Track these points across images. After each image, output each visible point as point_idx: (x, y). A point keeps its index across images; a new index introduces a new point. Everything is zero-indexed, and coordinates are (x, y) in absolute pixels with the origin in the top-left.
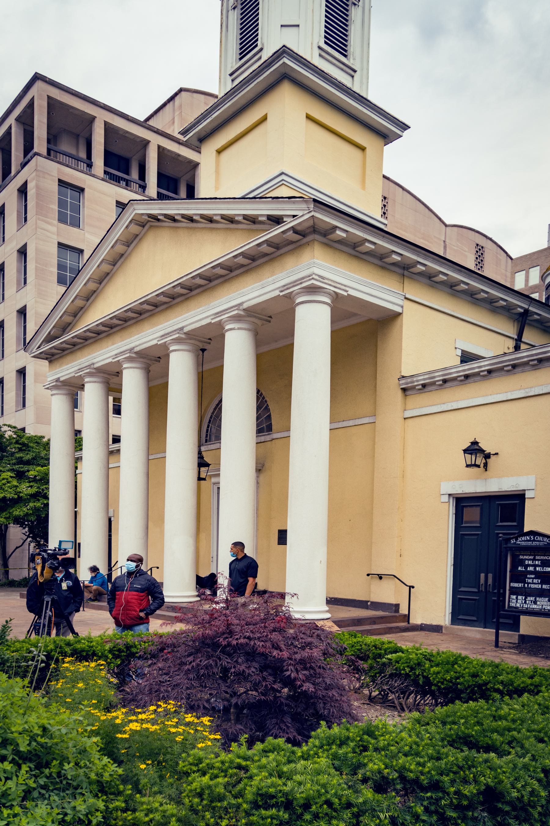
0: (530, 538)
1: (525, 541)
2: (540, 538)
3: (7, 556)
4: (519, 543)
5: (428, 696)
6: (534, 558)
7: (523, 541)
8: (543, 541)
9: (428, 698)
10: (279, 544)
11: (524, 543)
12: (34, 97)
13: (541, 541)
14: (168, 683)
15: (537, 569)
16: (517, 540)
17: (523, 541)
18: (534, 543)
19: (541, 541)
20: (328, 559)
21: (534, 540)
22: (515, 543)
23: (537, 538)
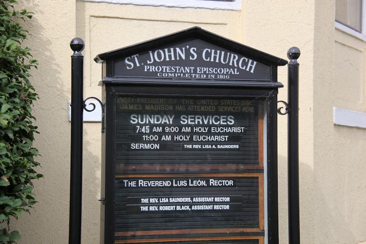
0: (188, 54)
1: (170, 63)
2: (217, 55)
3: (84, 100)
4: (153, 69)
5: (145, 209)
6: (160, 137)
7: (164, 63)
8: (227, 66)
9: (149, 204)
13: (220, 65)
15: (167, 201)
17: (164, 63)
19: (220, 65)
20: (315, 93)
21: (200, 62)
22: (138, 71)
23: (208, 55)
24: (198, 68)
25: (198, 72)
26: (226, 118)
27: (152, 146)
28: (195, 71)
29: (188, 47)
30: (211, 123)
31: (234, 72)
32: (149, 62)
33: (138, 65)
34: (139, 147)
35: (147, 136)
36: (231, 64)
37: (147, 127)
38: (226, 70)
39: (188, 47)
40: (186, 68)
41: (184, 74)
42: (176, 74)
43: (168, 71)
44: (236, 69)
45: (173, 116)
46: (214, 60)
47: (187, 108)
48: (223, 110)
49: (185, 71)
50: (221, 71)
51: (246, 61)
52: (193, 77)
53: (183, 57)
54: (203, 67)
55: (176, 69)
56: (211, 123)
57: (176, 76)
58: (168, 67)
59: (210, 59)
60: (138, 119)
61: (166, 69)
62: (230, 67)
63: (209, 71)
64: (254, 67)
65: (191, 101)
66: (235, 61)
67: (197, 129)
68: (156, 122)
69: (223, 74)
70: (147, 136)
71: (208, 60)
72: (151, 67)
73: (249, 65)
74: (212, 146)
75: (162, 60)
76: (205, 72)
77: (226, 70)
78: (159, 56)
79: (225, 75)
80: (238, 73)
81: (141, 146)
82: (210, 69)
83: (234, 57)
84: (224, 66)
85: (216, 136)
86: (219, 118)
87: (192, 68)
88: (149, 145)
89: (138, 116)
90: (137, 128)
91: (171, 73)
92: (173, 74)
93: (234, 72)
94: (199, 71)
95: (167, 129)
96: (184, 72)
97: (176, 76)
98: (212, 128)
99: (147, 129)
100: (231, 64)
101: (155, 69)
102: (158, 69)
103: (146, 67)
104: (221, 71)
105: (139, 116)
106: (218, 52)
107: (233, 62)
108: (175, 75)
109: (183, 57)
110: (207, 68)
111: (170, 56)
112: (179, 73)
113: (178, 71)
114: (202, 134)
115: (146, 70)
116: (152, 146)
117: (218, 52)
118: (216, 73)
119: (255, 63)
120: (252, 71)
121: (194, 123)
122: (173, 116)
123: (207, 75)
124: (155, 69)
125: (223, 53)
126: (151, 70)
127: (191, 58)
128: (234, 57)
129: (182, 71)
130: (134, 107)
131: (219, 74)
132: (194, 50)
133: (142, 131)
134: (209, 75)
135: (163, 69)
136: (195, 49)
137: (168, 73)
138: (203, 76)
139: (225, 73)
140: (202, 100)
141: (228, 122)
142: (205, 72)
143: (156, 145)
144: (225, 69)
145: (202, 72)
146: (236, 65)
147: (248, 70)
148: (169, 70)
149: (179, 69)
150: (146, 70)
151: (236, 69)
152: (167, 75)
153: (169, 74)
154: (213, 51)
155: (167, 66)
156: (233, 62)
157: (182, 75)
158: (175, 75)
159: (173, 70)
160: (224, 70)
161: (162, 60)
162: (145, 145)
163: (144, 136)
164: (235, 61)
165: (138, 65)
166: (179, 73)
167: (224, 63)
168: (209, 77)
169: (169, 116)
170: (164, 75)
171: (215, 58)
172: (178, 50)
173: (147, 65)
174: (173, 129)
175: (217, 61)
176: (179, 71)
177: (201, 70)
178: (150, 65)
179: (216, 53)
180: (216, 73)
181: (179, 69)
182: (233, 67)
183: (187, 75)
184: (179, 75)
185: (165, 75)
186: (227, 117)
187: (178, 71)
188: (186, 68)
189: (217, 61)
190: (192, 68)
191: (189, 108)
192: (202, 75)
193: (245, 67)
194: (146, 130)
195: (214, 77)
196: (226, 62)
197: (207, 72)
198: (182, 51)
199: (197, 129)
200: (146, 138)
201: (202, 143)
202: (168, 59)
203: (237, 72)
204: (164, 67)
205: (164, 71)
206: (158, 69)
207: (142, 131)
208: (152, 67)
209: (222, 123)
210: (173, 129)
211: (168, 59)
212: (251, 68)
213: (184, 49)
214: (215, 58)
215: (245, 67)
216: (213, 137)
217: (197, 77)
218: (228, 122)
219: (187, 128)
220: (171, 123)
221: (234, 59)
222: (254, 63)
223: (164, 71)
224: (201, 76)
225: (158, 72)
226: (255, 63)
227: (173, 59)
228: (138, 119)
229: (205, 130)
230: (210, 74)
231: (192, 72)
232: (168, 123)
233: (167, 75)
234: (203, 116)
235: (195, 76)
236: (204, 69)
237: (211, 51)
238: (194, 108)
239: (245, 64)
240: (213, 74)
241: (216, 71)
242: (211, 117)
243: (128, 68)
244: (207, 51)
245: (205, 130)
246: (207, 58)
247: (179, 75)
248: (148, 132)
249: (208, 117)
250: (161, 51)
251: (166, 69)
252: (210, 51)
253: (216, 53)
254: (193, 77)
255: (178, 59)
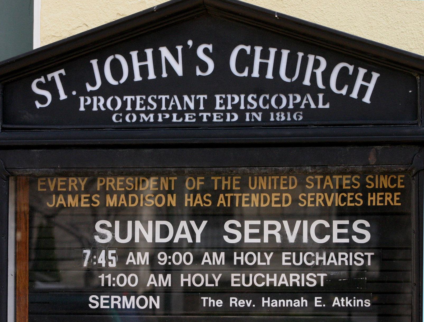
0: (191, 60)
1: (145, 88)
2: (270, 62)
4: (99, 104)
7: (131, 87)
8: (297, 88)
10: (338, 225)
11: (139, 109)
12: (292, 235)
14: (385, 8)
16: (77, 79)
17: (131, 87)
18: (227, 107)
19: (277, 86)
21: (223, 81)
23: (245, 61)
24: (218, 97)
25: (218, 108)
26: (350, 227)
27: (142, 302)
28: (210, 105)
29: (190, 43)
30: (305, 240)
31: (316, 103)
32: (89, 88)
33: (63, 96)
34: (109, 304)
35: (109, 276)
36: (307, 82)
37: (110, 252)
38: (295, 98)
39: (190, 43)
40: (186, 98)
41: (181, 114)
42: (160, 115)
43: (138, 108)
44: (321, 96)
45: (204, 223)
46: (260, 72)
47: (215, 199)
48: (314, 202)
49: (182, 106)
50: (279, 102)
51: (351, 73)
52: (205, 120)
53: (179, 69)
54: (293, 93)
55: (159, 102)
56: (305, 240)
57: (160, 120)
58: (138, 98)
59: (251, 71)
60: (112, 230)
61: (134, 103)
62: (303, 91)
63: (246, 102)
64: (371, 86)
65: (235, 182)
66: (319, 73)
67: (244, 259)
68: (159, 240)
69: (286, 110)
70: (109, 276)
71: (245, 74)
72: (95, 99)
73: (359, 82)
74: (311, 301)
75: (123, 81)
76: (236, 108)
77: (295, 98)
78: (116, 70)
79: (292, 111)
80: (327, 106)
81: (113, 302)
82: (250, 99)
83: (317, 64)
84: (288, 89)
85: (291, 275)
86: (327, 225)
87: (201, 97)
88: (133, 298)
89: (113, 224)
90: (86, 254)
91: (147, 113)
92: (151, 116)
93: (316, 103)
94: (221, 105)
95: (162, 256)
96: (179, 108)
97: (160, 120)
98: (284, 254)
99: (110, 257)
100: (307, 82)
101: (105, 105)
102: (114, 103)
103: (82, 99)
104: (279, 102)
105: (117, 223)
106: (273, 51)
107: (314, 75)
108: (156, 118)
109: (179, 69)
110: (243, 96)
111: (144, 70)
112: (167, 111)
113: (164, 108)
114: (255, 268)
115: (82, 109)
116: (142, 302)
117: (273, 51)
118: (267, 107)
119: (375, 76)
120: (367, 99)
121: (258, 241)
122: (204, 223)
123: (242, 114)
124: (105, 105)
125: (285, 53)
126: (95, 109)
127: (199, 73)
128: (317, 64)
129: (175, 106)
130: (80, 200)
131: (275, 111)
132: (206, 51)
133: (99, 262)
134: (248, 114)
135: (124, 104)
136: (210, 47)
137: (138, 113)
138: (232, 117)
139: (291, 106)
140: (382, 178)
141: (355, 238)
142: (236, 108)
143: (151, 298)
144: (291, 96)
145: (229, 107)
146: (320, 84)
147: (354, 95)
148: (141, 106)
149: (168, 102)
150: (82, 109)
151: (321, 96)
152: (135, 119)
153: (143, 115)
154: (258, 49)
155: (135, 95)
156: (314, 75)
157: (175, 115)
158: (156, 118)
159: (152, 106)
160: (98, 107)
161: (123, 81)
162: (125, 298)
163: (102, 276)
164: (319, 73)
165: (63, 96)
166: (167, 111)
167: (288, 80)
168: (248, 119)
169: (193, 223)
170: (127, 119)
171: (263, 67)
172: (165, 52)
173: (84, 96)
174: (177, 257)
175: (269, 76)
176: (167, 106)
177: (226, 101)
178: (92, 94)
179: (265, 55)
180: (267, 107)
181: (168, 102)
182: (313, 90)
183: (187, 115)
184: (167, 116)
185: (131, 118)
186: (351, 223)
187: (164, 108)
188: (186, 98)
189: (269, 76)
190: (202, 97)
191: (221, 201)
192: (228, 115)
193: (346, 87)
194: (107, 260)
195: (259, 119)
196: (294, 79)
197: (242, 107)
198: (175, 54)
199: (244, 259)
200: (106, 280)
201: (255, 293)
202: (138, 78)
203: (324, 104)
204: (129, 98)
205: (129, 108)
206: (114, 103)
207: (99, 262)
208: (99, 101)
209: (336, 240)
210: (177, 257)
211: (138, 78)
212: (363, 89)
213: (179, 48)
214: (263, 67)
215: (346, 87)
216: (283, 275)
217: (215, 120)
218: (355, 238)
219: (215, 254)
220: (198, 240)
221: (315, 68)
222: (371, 76)
223: (129, 108)
224: (225, 117)
225: (114, 112)
226: (375, 76)
227: (152, 76)
228: (112, 230)
229: (264, 259)
230: (250, 111)
231: (202, 108)
232: (190, 240)
233: (135, 119)
234: (285, 223)
235: (210, 119)
236: (233, 99)
237: (253, 51)
238: (233, 199)
239: (346, 79)
240: (258, 109)
241: (266, 102)
242: (305, 223)
243: (38, 105)
244: (242, 52)
245: (264, 259)
246: (240, 70)
247: (167, 116)
248: (113, 265)
249: (298, 223)
250: (120, 57)
251: (134, 103)
252: (248, 52)
253: (265, 55)
254: (205, 120)
255: (165, 75)
